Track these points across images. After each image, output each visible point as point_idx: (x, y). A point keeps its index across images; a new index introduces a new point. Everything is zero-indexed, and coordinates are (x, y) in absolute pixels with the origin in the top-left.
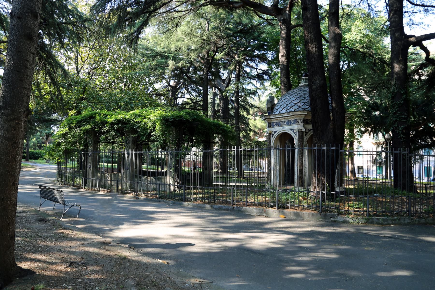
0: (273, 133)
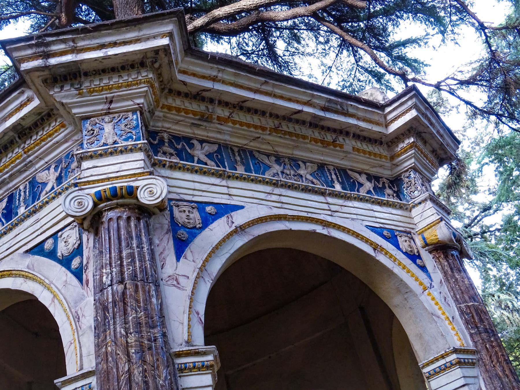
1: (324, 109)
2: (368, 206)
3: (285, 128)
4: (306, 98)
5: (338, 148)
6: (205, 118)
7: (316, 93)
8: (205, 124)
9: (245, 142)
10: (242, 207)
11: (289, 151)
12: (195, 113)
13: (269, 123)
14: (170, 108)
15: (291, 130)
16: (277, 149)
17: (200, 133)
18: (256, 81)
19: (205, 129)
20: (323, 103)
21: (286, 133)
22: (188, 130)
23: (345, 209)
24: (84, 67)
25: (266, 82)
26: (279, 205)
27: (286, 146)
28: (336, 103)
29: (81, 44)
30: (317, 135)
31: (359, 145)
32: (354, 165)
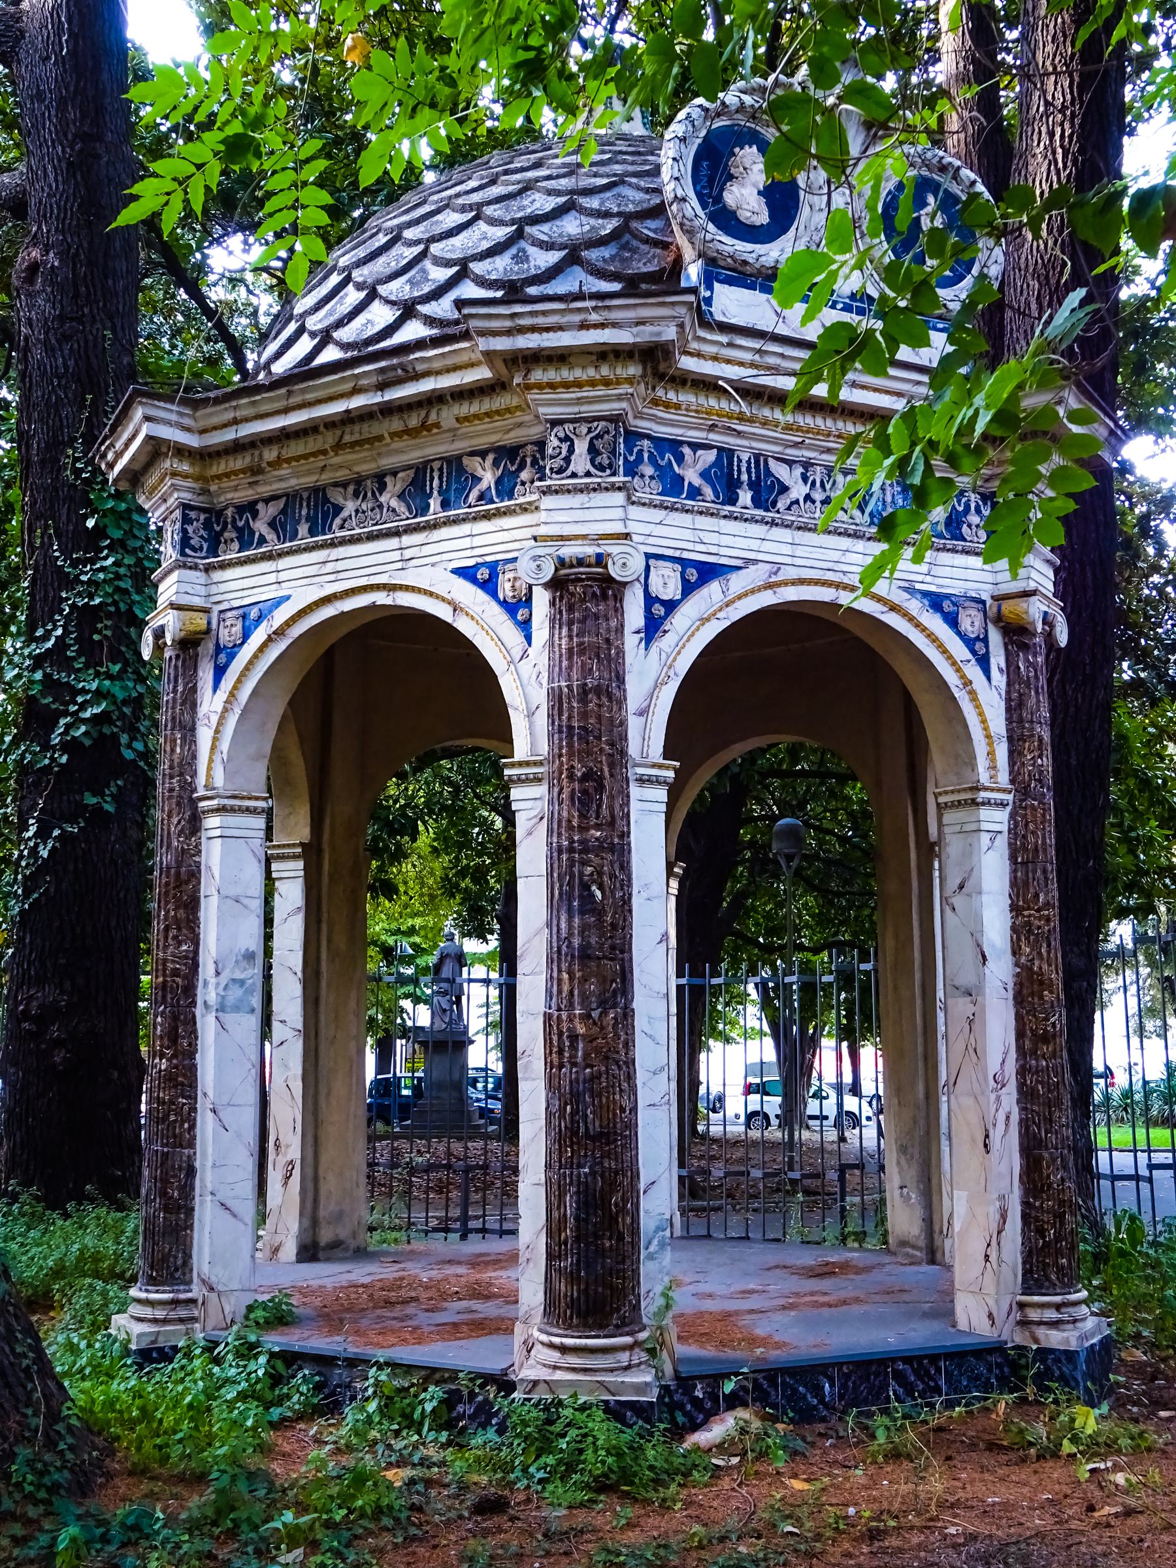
0: (666, 582)
1: (382, 387)
2: (466, 528)
3: (347, 438)
4: (348, 386)
5: (435, 431)
6: (255, 471)
7: (357, 371)
8: (260, 477)
9: (314, 478)
10: (288, 598)
11: (373, 465)
12: (243, 471)
13: (328, 439)
14: (218, 477)
15: (356, 437)
16: (357, 469)
17: (265, 490)
18: (278, 398)
19: (266, 483)
20: (373, 380)
21: (353, 445)
22: (250, 492)
23: (427, 550)
24: (137, 467)
25: (290, 393)
26: (332, 577)
27: (364, 461)
28: (393, 368)
29: (119, 445)
30: (396, 424)
31: (464, 409)
32: (475, 442)
